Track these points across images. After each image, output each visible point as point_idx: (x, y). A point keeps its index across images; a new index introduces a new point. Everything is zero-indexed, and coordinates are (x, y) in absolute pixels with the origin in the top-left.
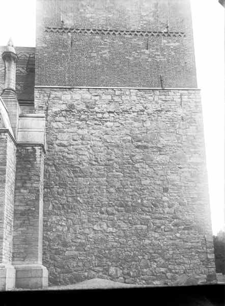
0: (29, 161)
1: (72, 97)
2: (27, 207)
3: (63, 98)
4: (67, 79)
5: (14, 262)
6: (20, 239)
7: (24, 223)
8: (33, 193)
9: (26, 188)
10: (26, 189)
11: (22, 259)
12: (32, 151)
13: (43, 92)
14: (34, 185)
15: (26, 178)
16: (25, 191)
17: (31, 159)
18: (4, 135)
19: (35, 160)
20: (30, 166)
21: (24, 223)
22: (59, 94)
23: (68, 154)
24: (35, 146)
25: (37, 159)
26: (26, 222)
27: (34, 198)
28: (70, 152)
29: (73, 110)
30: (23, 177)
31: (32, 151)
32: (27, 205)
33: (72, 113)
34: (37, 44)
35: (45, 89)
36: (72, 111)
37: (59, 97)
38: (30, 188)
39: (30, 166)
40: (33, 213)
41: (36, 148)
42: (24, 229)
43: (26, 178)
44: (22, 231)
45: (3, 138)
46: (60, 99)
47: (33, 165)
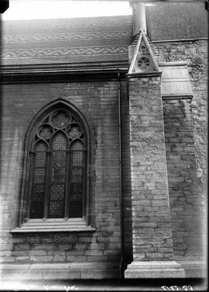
0: (177, 118)
1: (197, 50)
2: (181, 179)
3: (186, 52)
4: (188, 31)
5: (14, 253)
6: (176, 224)
7: (179, 201)
8: (186, 160)
9: (176, 154)
10: (177, 154)
11: (182, 253)
12: (179, 105)
13: (162, 47)
14: (187, 149)
15: (174, 140)
16: (175, 157)
17: (179, 116)
18: (156, 80)
19: (185, 117)
20: (178, 124)
21: (179, 201)
22: (181, 48)
23: (199, 116)
24: (183, 99)
25: (187, 115)
26: (181, 199)
27: (189, 167)
28: (201, 113)
29: (200, 65)
30: (171, 139)
31: (179, 105)
32: (180, 176)
33: (200, 68)
34: (14, 47)
35: (165, 44)
36: (199, 67)
37: (181, 52)
38: (182, 153)
39: (178, 124)
40: (190, 186)
41: (184, 101)
42: (180, 209)
43: (174, 140)
44: (177, 212)
45: (155, 84)
46: (184, 54)
47: (182, 124)
